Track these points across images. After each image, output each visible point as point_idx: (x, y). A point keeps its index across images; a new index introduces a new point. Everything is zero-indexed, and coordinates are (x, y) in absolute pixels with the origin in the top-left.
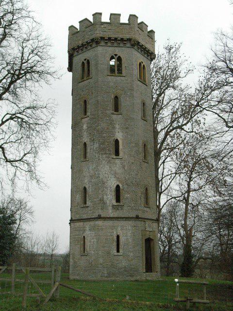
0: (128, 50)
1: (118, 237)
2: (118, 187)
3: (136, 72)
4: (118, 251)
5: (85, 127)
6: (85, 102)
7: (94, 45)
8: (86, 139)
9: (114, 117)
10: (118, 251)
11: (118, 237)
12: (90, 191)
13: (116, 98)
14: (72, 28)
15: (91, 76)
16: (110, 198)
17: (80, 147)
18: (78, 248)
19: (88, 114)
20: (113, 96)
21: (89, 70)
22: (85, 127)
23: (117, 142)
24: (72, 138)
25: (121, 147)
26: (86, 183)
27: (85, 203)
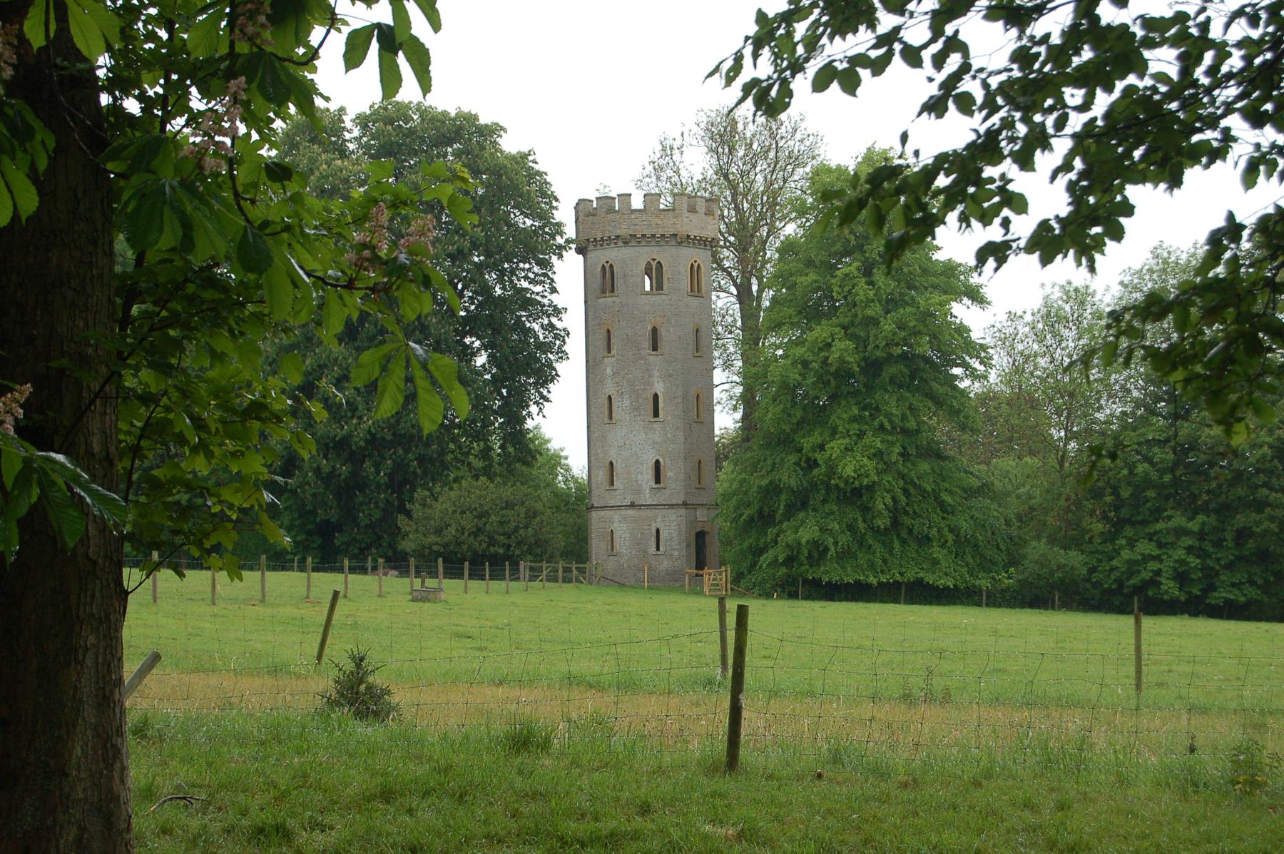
0: (673, 250)
1: (658, 531)
2: (657, 462)
3: (685, 283)
4: (658, 549)
5: (609, 371)
6: (608, 331)
7: (620, 244)
8: (610, 388)
9: (652, 359)
10: (658, 549)
11: (658, 531)
12: (618, 467)
13: (654, 330)
14: (581, 208)
15: (616, 293)
16: (647, 476)
17: (299, 284)
18: (602, 476)
19: (614, 352)
20: (649, 328)
21: (613, 280)
22: (609, 371)
23: (656, 397)
24: (847, 599)
25: (661, 405)
26: (613, 455)
27: (612, 484)
